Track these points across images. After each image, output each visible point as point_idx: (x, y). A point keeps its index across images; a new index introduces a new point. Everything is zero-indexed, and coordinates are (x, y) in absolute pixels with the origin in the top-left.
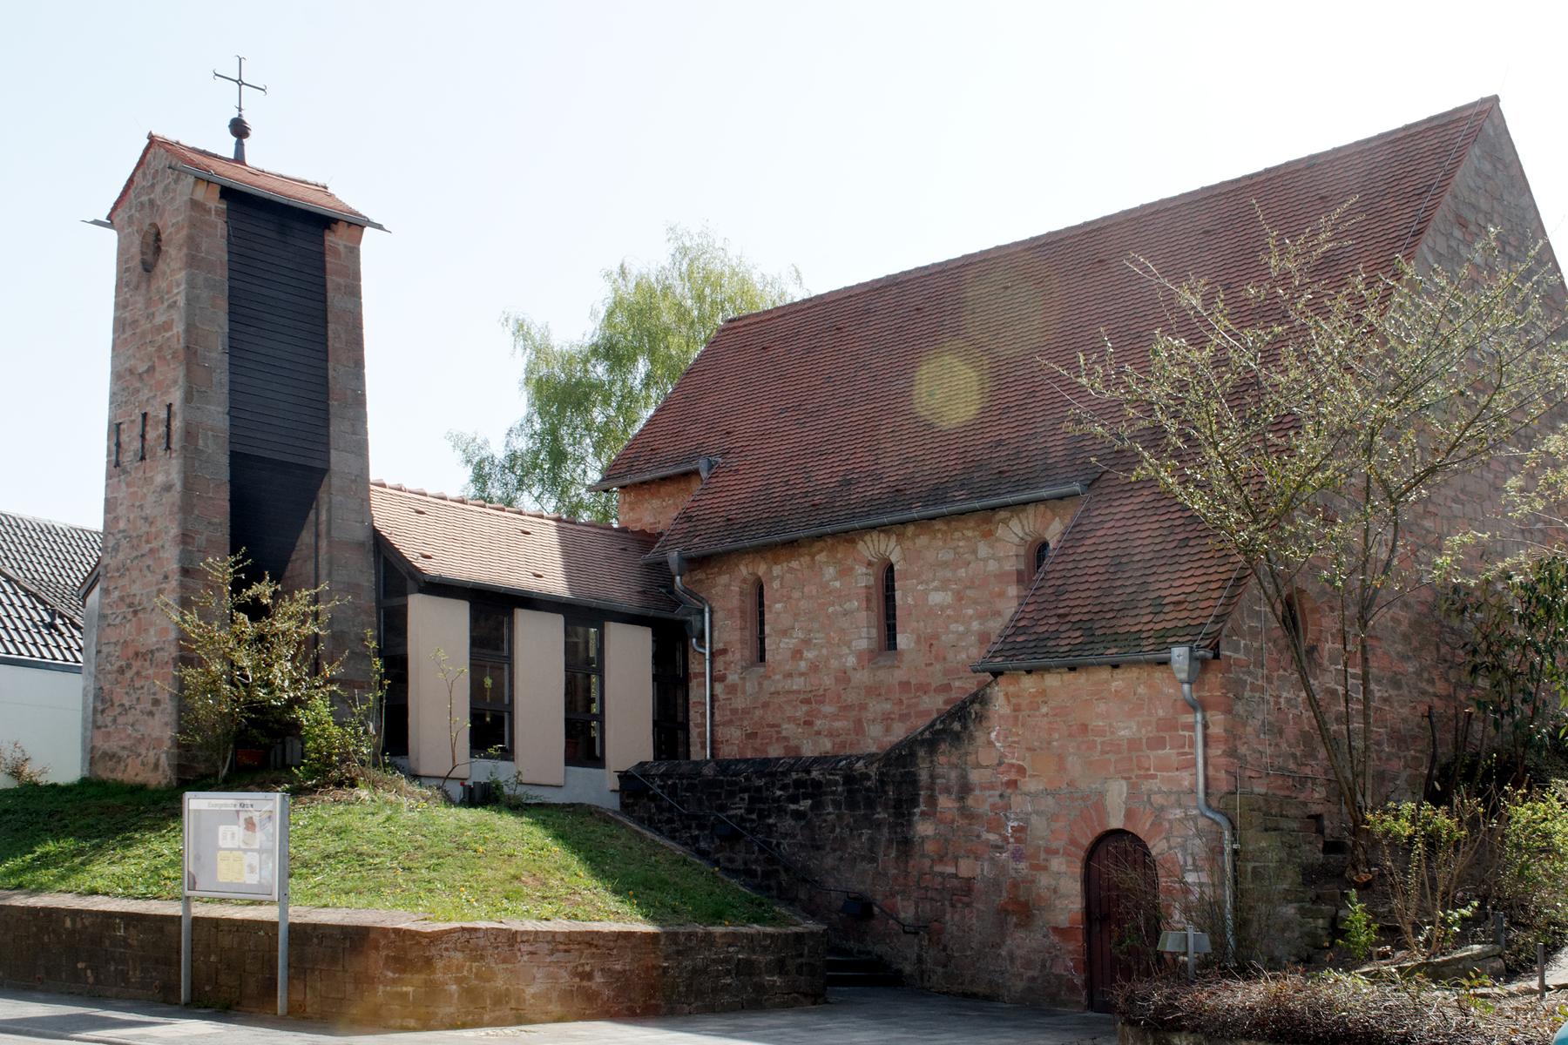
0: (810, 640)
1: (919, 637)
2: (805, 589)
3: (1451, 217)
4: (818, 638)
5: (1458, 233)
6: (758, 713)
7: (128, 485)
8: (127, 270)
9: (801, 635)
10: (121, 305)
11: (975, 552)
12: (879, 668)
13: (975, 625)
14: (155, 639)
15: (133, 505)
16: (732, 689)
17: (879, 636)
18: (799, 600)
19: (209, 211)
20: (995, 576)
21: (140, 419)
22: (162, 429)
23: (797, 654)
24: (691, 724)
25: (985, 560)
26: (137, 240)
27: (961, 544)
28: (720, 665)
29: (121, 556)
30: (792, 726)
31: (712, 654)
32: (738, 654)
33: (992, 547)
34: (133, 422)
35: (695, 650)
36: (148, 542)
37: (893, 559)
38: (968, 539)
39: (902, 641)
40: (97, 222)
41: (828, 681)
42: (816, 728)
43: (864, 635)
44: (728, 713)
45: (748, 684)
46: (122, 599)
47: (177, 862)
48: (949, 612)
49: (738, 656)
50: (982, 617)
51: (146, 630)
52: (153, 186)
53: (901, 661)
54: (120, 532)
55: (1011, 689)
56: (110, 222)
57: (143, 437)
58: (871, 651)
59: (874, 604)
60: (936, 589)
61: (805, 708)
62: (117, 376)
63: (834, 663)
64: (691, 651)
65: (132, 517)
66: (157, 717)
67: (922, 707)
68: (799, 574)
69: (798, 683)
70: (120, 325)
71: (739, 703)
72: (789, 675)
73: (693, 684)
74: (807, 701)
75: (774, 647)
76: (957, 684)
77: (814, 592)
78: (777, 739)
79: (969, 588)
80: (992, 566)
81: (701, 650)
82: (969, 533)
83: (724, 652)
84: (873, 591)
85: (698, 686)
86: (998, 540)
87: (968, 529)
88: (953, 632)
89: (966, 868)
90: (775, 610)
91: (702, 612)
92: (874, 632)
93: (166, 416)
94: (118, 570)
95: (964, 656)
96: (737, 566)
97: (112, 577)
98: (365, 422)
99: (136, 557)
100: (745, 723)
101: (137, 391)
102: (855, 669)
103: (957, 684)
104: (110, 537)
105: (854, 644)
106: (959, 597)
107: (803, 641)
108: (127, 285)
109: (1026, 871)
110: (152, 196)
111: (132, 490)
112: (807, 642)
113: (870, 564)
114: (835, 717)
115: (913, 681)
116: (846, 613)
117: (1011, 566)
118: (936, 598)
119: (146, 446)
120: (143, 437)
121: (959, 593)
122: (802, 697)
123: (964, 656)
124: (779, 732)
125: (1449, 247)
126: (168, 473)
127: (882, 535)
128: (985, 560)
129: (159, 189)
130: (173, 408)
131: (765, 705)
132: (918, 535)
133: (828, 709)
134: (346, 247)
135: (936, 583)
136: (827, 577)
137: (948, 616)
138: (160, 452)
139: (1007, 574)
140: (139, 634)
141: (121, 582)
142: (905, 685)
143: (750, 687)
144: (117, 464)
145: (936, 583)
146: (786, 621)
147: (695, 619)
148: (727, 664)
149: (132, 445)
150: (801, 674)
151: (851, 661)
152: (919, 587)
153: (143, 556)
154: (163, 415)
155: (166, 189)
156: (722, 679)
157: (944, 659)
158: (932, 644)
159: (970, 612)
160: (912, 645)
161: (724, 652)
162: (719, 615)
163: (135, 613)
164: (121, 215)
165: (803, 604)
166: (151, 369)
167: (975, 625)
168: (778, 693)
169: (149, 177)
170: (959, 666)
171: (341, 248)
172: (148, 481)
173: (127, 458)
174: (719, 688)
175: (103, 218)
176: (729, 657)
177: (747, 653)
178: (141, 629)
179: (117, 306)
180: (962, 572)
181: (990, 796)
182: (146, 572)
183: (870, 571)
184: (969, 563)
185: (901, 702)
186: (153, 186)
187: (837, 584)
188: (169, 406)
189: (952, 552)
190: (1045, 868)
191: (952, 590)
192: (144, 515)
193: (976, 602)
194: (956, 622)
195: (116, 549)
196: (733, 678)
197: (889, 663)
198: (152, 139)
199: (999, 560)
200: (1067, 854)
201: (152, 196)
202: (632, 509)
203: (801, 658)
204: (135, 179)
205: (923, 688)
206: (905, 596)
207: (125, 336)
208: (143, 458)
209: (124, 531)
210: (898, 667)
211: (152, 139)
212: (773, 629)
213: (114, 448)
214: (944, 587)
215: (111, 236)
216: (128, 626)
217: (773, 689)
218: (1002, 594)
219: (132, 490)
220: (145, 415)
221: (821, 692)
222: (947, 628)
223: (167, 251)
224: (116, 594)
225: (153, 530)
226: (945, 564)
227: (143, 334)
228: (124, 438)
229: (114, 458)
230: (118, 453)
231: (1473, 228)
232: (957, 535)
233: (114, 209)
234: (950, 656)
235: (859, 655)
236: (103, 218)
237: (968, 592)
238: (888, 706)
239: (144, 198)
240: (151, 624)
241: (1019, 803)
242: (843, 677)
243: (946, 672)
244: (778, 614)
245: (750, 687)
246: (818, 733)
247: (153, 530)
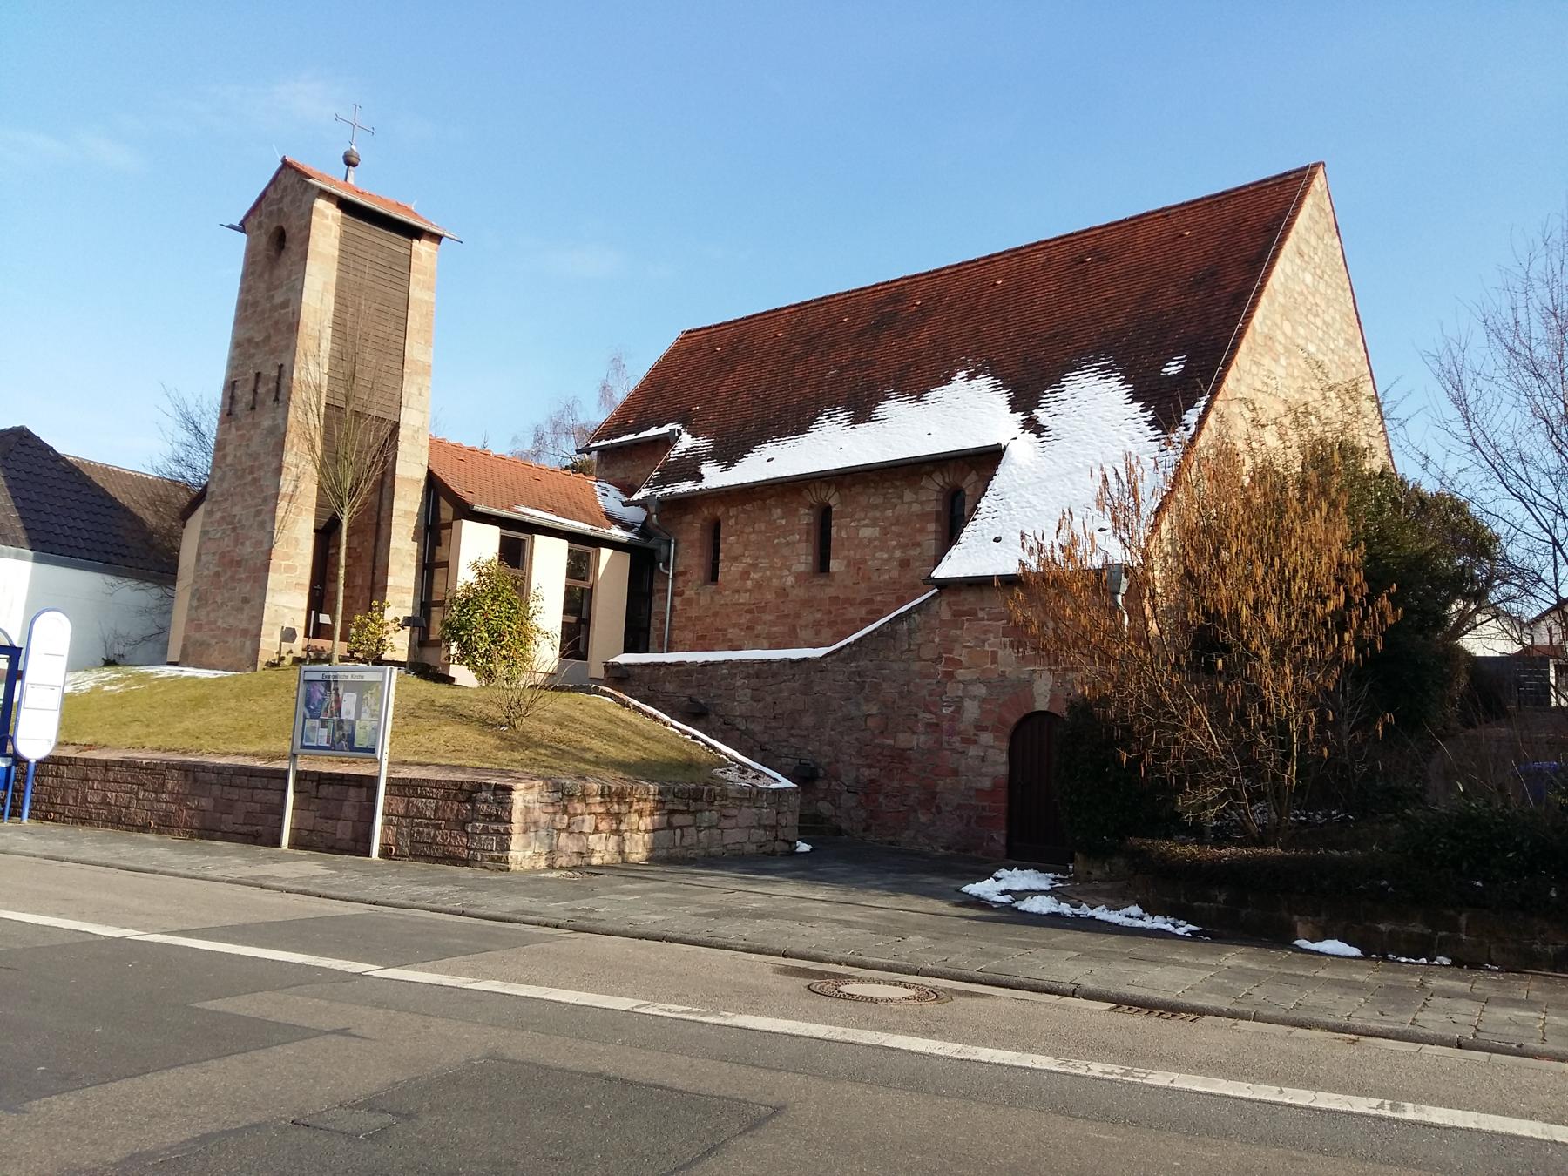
0: (757, 565)
1: (849, 562)
2: (756, 526)
3: (1295, 248)
4: (764, 563)
5: (1298, 261)
6: (708, 620)
7: (237, 430)
8: (253, 263)
9: (749, 560)
10: (245, 289)
11: (901, 497)
12: (813, 586)
13: (898, 553)
14: (250, 550)
15: (240, 445)
16: (689, 602)
17: (814, 561)
18: (750, 533)
19: (327, 217)
20: (917, 515)
21: (253, 377)
22: (272, 385)
23: (745, 575)
24: (652, 629)
25: (910, 503)
26: (264, 239)
27: (890, 491)
28: (680, 583)
29: (226, 485)
30: (737, 630)
31: (673, 575)
32: (697, 575)
33: (916, 494)
34: (247, 380)
35: (660, 571)
36: (251, 473)
37: (832, 502)
38: (896, 487)
39: (835, 565)
40: (232, 227)
41: (769, 596)
42: (756, 632)
43: (803, 560)
44: (683, 620)
45: (702, 598)
46: (223, 518)
47: (60, 744)
48: (877, 543)
49: (695, 577)
50: (903, 547)
51: (242, 544)
52: (282, 198)
53: (833, 580)
54: (227, 466)
55: (953, 599)
56: (243, 227)
57: (255, 391)
58: (808, 573)
59: (812, 538)
60: (866, 526)
61: (748, 616)
62: (237, 344)
63: (775, 582)
64: (656, 572)
65: (238, 454)
66: (245, 612)
67: (849, 616)
68: (752, 515)
69: (744, 598)
70: (243, 306)
71: (693, 612)
72: (738, 591)
73: (656, 597)
74: (750, 611)
75: (726, 569)
76: (879, 598)
77: (763, 528)
78: (723, 641)
79: (894, 525)
80: (916, 508)
81: (666, 572)
82: (898, 483)
83: (684, 573)
84: (812, 527)
85: (660, 599)
86: (922, 488)
87: (897, 480)
88: (878, 559)
89: (904, 740)
90: (729, 542)
91: (669, 543)
92: (810, 558)
93: (276, 374)
94: (222, 495)
95: (886, 577)
96: (700, 508)
97: (216, 501)
98: (27, 602)
99: (240, 485)
100: (698, 627)
101: (252, 356)
102: (793, 587)
103: (879, 598)
104: (218, 470)
105: (793, 567)
106: (885, 531)
107: (750, 565)
108: (252, 274)
109: (957, 744)
110: (280, 206)
111: (240, 433)
112: (754, 566)
113: (812, 506)
114: (773, 624)
115: (841, 597)
116: (788, 544)
117: (931, 508)
118: (865, 532)
119: (257, 398)
120: (255, 391)
121: (885, 528)
122: (746, 608)
123: (886, 577)
124: (726, 635)
125: (1293, 270)
126: (274, 419)
127: (824, 485)
128: (910, 503)
129: (287, 200)
130: (283, 368)
131: (715, 614)
132: (854, 485)
133: (768, 617)
134: (427, 252)
135: (866, 521)
136: (775, 516)
137: (875, 547)
138: (269, 402)
139: (929, 514)
140: (236, 545)
141: (224, 505)
142: (834, 599)
143: (704, 600)
144: (229, 414)
145: (866, 521)
146: (738, 550)
147: (664, 548)
148: (686, 583)
149: (245, 395)
150: (746, 591)
151: (790, 580)
152: (852, 524)
153: (245, 484)
154: (275, 373)
155: (293, 201)
156: (681, 594)
157: (870, 579)
158: (859, 568)
159: (894, 543)
160: (843, 568)
161: (684, 573)
162: (682, 545)
163: (234, 529)
164: (254, 221)
165: (753, 537)
166: (268, 338)
167: (898, 553)
168: (727, 604)
169: (280, 191)
170: (882, 585)
171: (423, 253)
172: (255, 425)
173: (240, 408)
174: (678, 601)
175: (236, 223)
176: (688, 577)
177: (702, 574)
178: (238, 541)
179: (242, 291)
180: (889, 513)
181: (929, 684)
182: (247, 496)
183: (811, 512)
184: (896, 506)
185: (830, 612)
186: (282, 198)
187: (784, 522)
188: (281, 366)
189: (882, 498)
190: (975, 742)
191: (880, 526)
192: (249, 452)
193: (899, 535)
194: (881, 551)
195: (222, 479)
196: (689, 593)
197: (822, 582)
198: (286, 165)
199: (921, 503)
200: (996, 730)
201: (280, 206)
202: (606, 468)
203: (748, 579)
204: (268, 193)
205: (849, 601)
206: (839, 531)
207: (247, 313)
208: (253, 408)
209: (231, 465)
210: (830, 585)
211: (286, 165)
212: (725, 556)
213: (228, 401)
214: (874, 524)
215: (242, 238)
216: (226, 539)
217: (722, 602)
218: (922, 530)
219: (240, 433)
220: (258, 375)
221: (763, 604)
222: (874, 555)
223: (289, 248)
224: (219, 515)
225: (257, 463)
226: (876, 507)
227: (263, 312)
228: (238, 392)
229: (227, 408)
230: (231, 404)
231: (1306, 258)
232: (887, 484)
233: (246, 217)
234: (875, 577)
235: (798, 576)
236: (236, 223)
237: (893, 528)
238: (818, 615)
239: (275, 207)
240: (248, 538)
241: (954, 690)
242: (783, 593)
243: (870, 589)
244: (732, 544)
245: (704, 600)
246: (758, 636)
247: (257, 463)
